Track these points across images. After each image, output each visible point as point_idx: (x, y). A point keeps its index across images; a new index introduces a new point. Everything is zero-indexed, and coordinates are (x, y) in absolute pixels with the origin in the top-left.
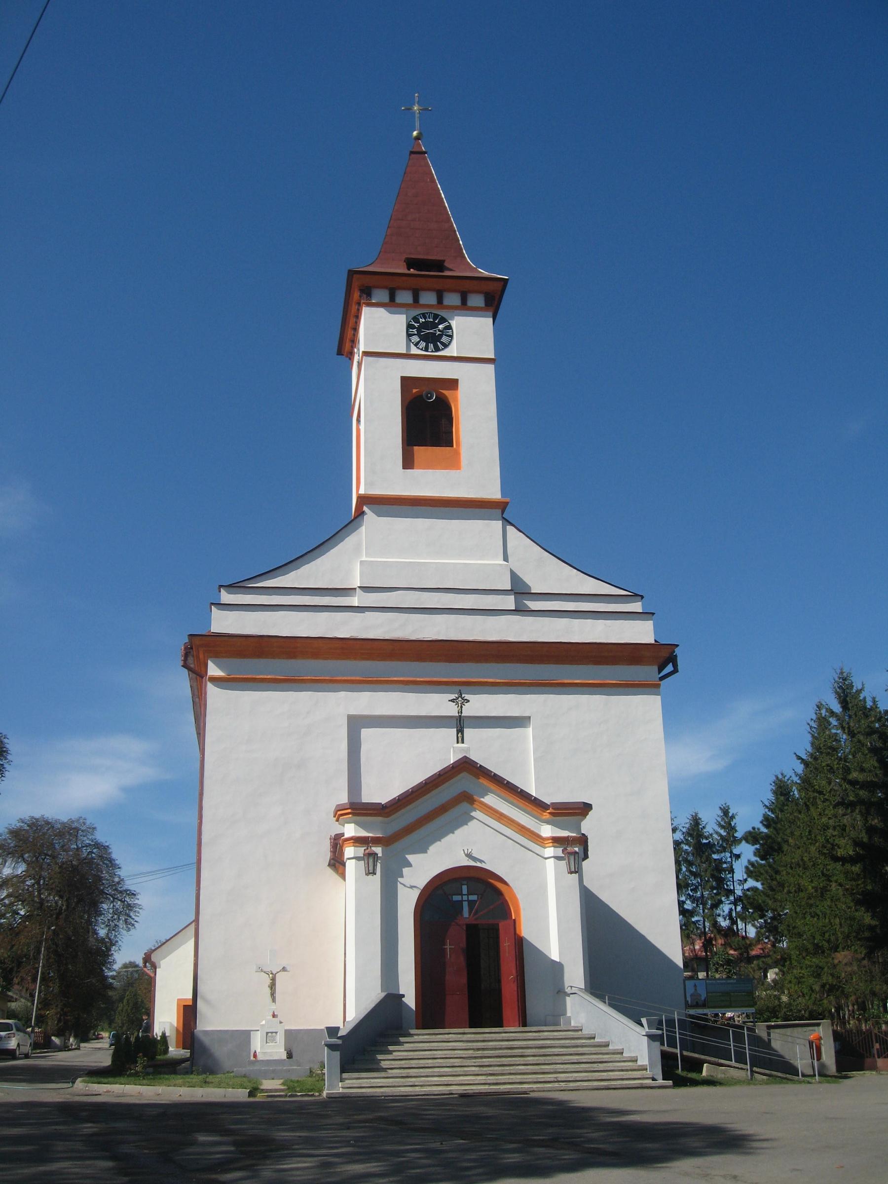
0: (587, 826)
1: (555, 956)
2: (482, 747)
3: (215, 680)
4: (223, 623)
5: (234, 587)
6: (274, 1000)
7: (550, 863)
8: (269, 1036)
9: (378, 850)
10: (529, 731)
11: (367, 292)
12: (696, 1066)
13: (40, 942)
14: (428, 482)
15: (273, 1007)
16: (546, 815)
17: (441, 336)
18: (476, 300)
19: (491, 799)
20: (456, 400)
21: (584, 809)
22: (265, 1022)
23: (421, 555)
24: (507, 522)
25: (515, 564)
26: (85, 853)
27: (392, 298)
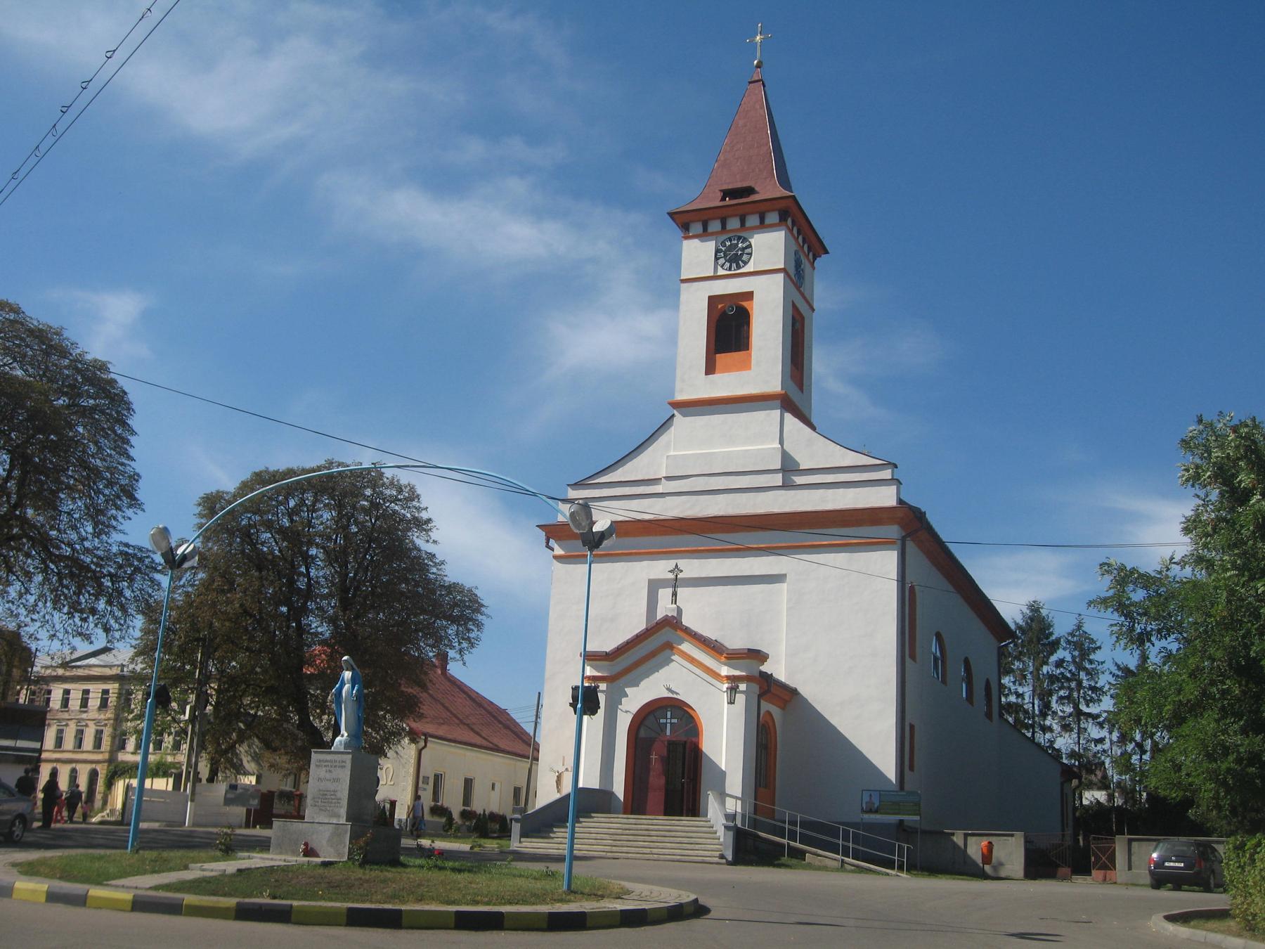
2: (699, 609)
5: (577, 485)
10: (784, 586)
14: (727, 384)
18: (773, 218)
19: (686, 647)
27: (705, 229)
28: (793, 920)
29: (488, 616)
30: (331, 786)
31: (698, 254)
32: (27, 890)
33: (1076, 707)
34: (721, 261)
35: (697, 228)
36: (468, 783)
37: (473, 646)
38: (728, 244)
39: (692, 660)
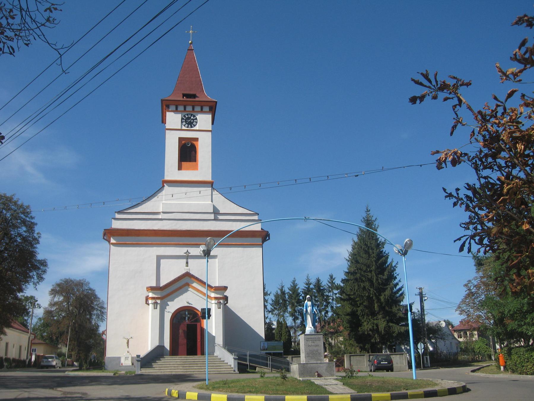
0: (226, 294)
1: (214, 335)
2: (197, 267)
3: (113, 244)
4: (116, 225)
5: (119, 212)
6: (128, 347)
7: (214, 305)
8: (126, 358)
9: (159, 301)
10: (217, 260)
11: (168, 107)
12: (255, 368)
13: (68, 327)
14: (187, 175)
15: (128, 349)
16: (213, 290)
18: (206, 109)
19: (195, 285)
21: (225, 288)
22: (125, 354)
23: (184, 201)
24: (213, 189)
25: (215, 203)
26: (85, 293)
27: (177, 108)
28: (421, 391)
30: (316, 348)
35: (173, 108)
38: (187, 116)
39: (198, 291)
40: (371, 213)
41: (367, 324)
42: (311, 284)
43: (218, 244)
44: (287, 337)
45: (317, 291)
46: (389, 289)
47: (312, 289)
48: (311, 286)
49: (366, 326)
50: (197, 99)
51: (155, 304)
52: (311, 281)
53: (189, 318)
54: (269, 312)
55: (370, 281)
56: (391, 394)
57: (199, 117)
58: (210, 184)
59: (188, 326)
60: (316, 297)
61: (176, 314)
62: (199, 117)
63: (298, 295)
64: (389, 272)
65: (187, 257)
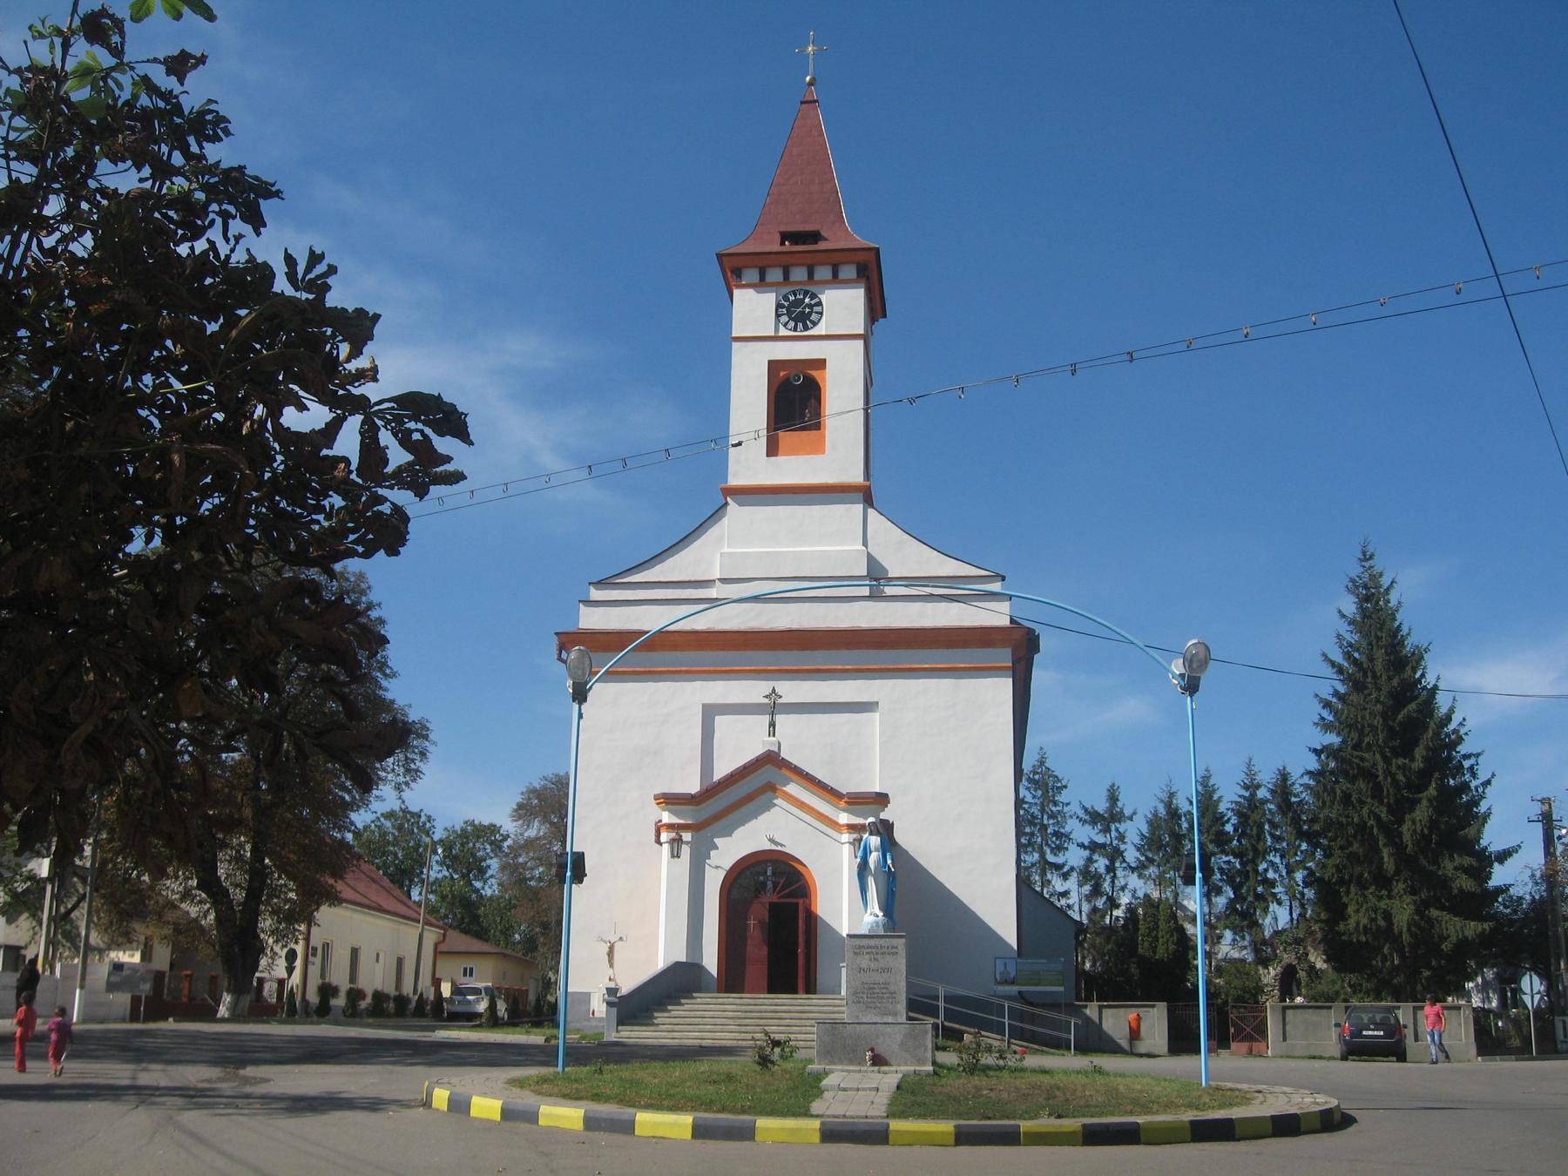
2: (800, 741)
4: (592, 619)
5: (601, 584)
6: (611, 965)
9: (687, 836)
11: (737, 273)
14: (793, 469)
15: (610, 972)
16: (842, 804)
17: (810, 314)
18: (848, 272)
19: (793, 789)
20: (824, 379)
23: (781, 547)
27: (762, 278)
28: (1072, 1124)
29: (435, 743)
30: (880, 978)
31: (753, 309)
32: (783, 1129)
33: (1043, 855)
34: (784, 319)
35: (751, 275)
36: (355, 952)
37: (414, 780)
38: (792, 298)
39: (801, 805)
40: (1378, 564)
41: (1357, 911)
42: (1258, 786)
43: (607, 672)
44: (1172, 947)
45: (1279, 807)
46: (1424, 802)
47: (1264, 802)
48: (1262, 793)
49: (1356, 918)
50: (822, 246)
51: (676, 842)
52: (1258, 778)
53: (775, 885)
54: (1133, 869)
55: (1369, 775)
56: (957, 1127)
57: (829, 297)
58: (865, 495)
59: (774, 908)
60: (1274, 826)
61: (738, 876)
62: (829, 297)
63: (1220, 819)
64: (1428, 748)
65: (773, 708)
